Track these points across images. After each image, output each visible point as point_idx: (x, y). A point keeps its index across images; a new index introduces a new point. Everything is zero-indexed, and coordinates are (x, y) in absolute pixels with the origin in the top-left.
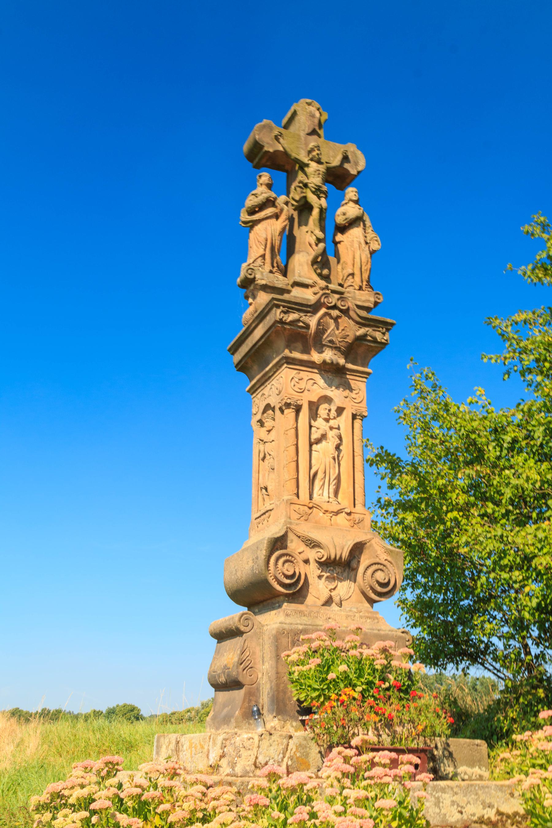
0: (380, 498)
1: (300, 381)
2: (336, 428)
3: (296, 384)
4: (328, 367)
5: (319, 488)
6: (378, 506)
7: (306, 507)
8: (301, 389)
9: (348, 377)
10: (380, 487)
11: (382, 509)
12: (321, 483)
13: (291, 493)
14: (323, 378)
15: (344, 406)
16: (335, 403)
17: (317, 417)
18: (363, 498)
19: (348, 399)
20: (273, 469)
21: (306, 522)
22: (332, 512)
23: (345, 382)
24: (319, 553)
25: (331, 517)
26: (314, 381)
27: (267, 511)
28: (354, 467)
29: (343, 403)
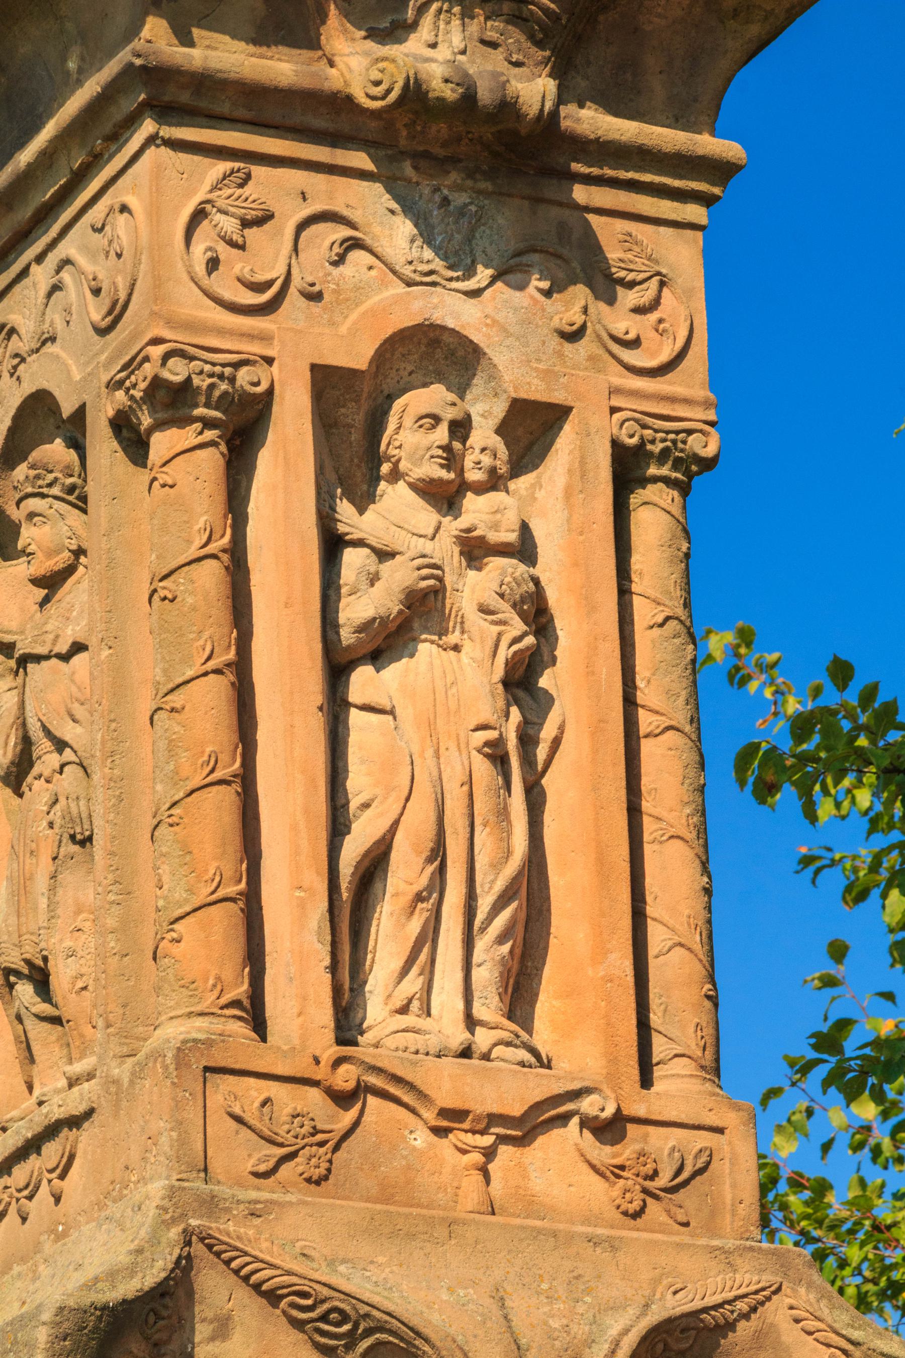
0: (844, 1025)
1: (252, 234)
2: (503, 550)
3: (224, 251)
4: (440, 129)
5: (397, 964)
6: (822, 1071)
7: (314, 1094)
8: (259, 287)
9: (580, 194)
10: (838, 951)
11: (851, 1094)
12: (415, 926)
13: (209, 1001)
14: (409, 208)
15: (558, 397)
16: (494, 376)
17: (376, 479)
18: (705, 1019)
19: (585, 346)
20: (86, 841)
21: (312, 1196)
22: (494, 1119)
23: (563, 231)
25: (490, 1153)
26: (345, 232)
27: (51, 1131)
28: (634, 811)
29: (548, 375)
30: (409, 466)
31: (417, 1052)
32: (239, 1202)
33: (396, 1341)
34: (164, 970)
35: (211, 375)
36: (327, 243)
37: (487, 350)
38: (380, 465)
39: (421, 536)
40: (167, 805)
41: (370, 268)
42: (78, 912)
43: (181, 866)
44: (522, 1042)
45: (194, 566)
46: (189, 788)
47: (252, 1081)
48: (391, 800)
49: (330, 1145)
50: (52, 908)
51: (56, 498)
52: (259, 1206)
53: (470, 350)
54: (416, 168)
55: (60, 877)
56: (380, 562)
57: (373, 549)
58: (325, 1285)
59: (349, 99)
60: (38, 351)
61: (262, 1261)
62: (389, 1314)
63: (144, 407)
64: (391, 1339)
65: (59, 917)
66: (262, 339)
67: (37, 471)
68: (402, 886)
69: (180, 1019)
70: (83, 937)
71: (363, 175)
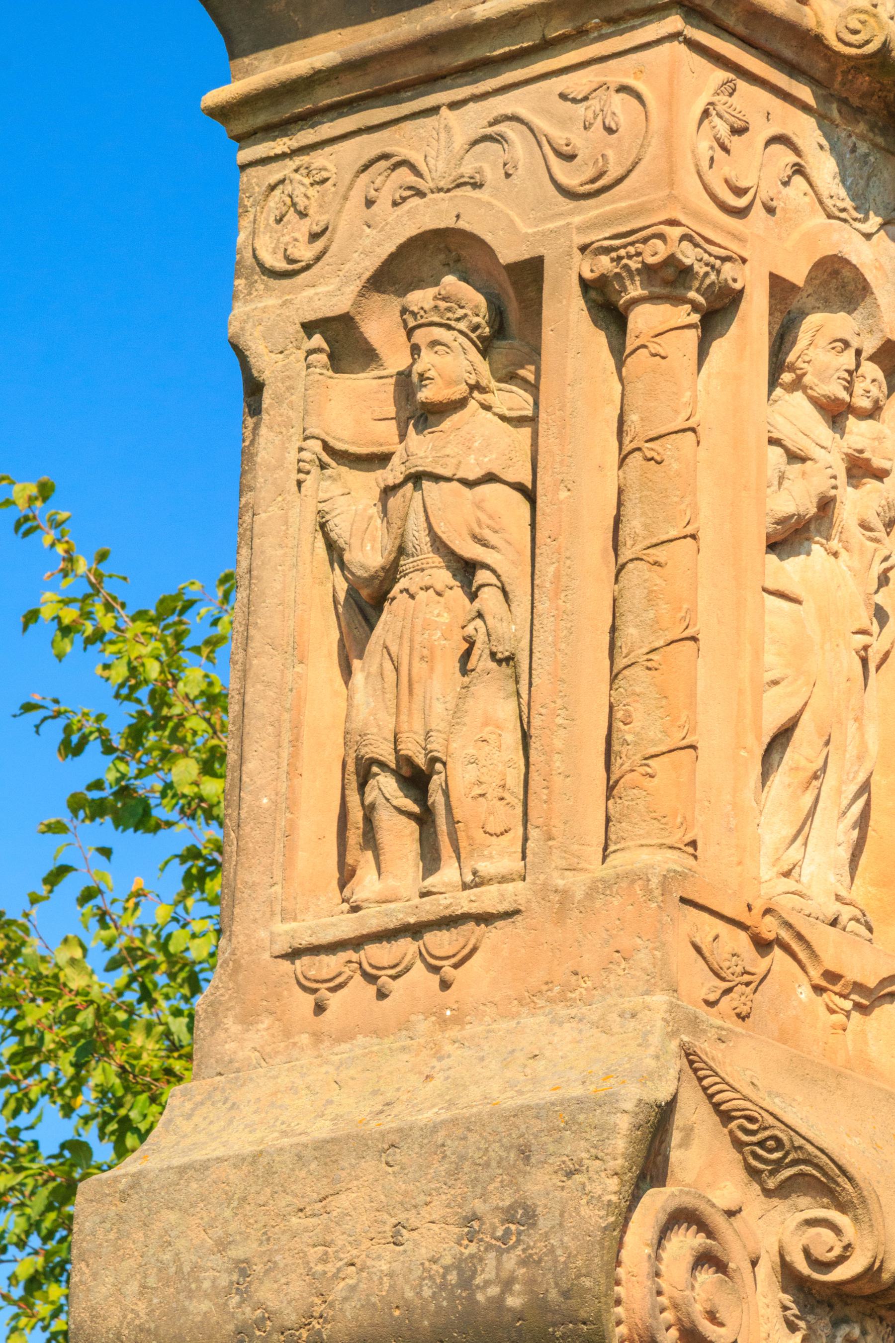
7: (743, 936)
22: (858, 987)
24: (827, 1234)
30: (816, 381)
31: (809, 916)
32: (712, 1026)
33: (818, 1175)
34: (632, 800)
35: (707, 265)
36: (783, 165)
37: (875, 290)
38: (783, 371)
39: (822, 447)
40: (646, 650)
41: (805, 194)
42: (486, 724)
43: (657, 708)
44: (866, 922)
45: (680, 435)
46: (670, 638)
47: (706, 916)
48: (799, 682)
49: (753, 986)
50: (458, 715)
51: (461, 332)
52: (724, 1033)
53: (860, 287)
54: (840, 112)
55: (472, 689)
56: (789, 463)
57: (787, 451)
58: (771, 1114)
59: (819, 39)
60: (448, 190)
61: (727, 1084)
62: (822, 1151)
63: (637, 278)
64: (814, 1172)
65: (465, 724)
66: (740, 240)
67: (449, 304)
68: (803, 763)
69: (650, 849)
70: (487, 748)
71: (805, 108)
